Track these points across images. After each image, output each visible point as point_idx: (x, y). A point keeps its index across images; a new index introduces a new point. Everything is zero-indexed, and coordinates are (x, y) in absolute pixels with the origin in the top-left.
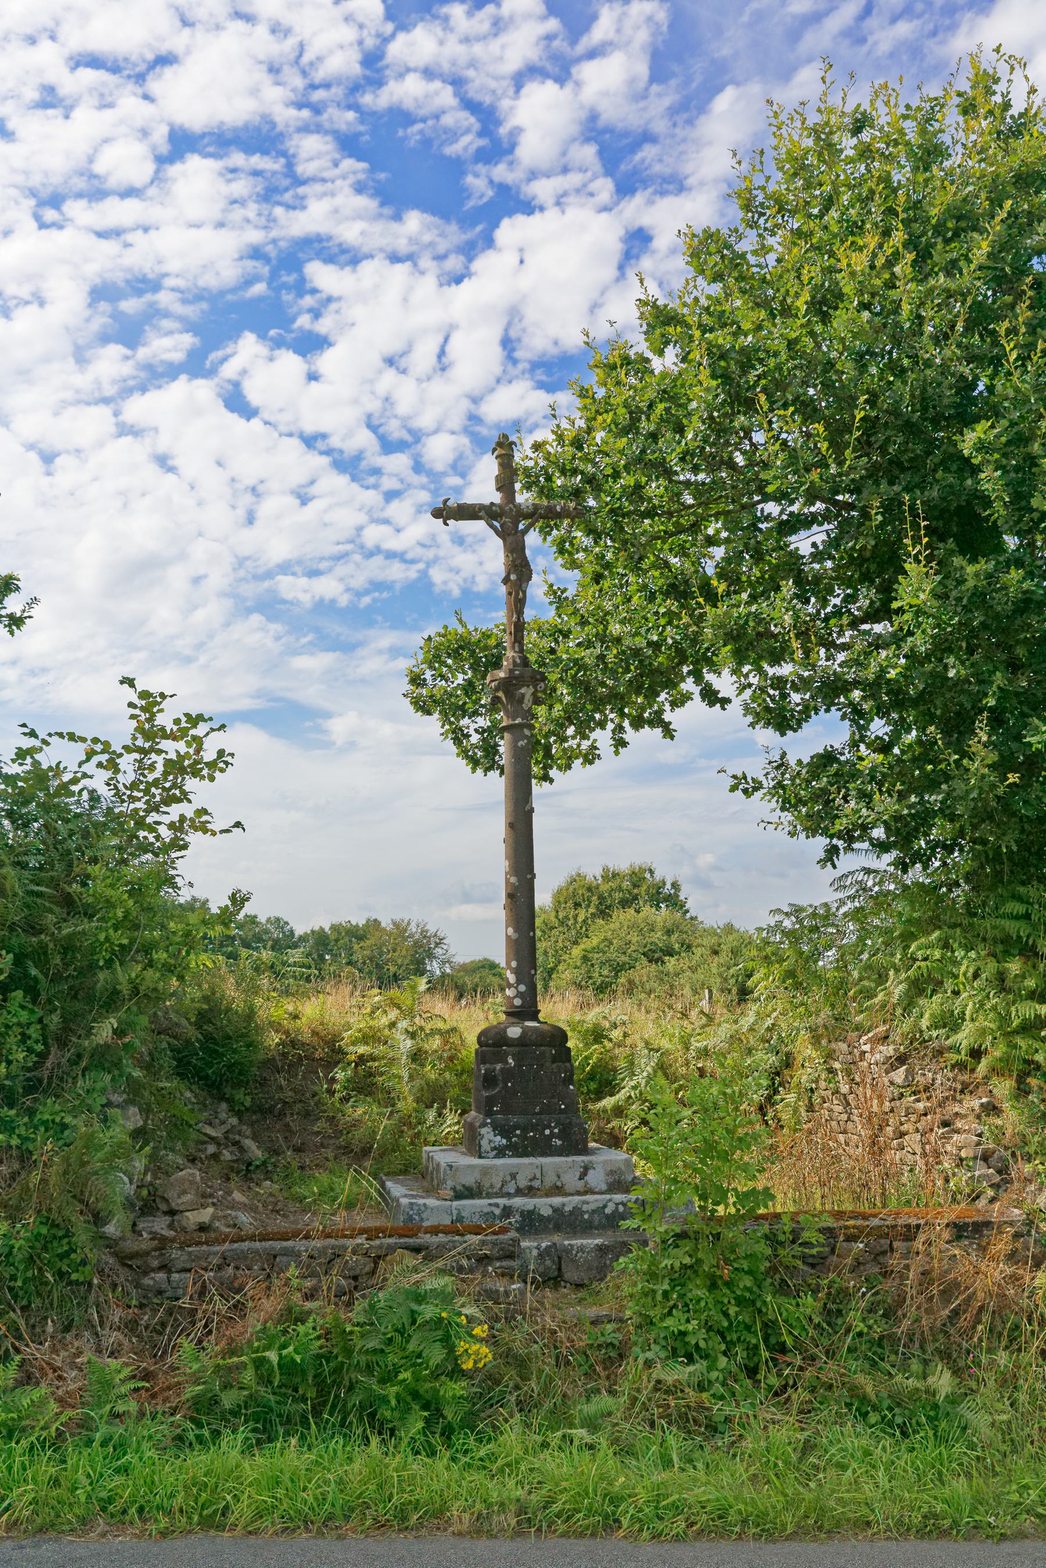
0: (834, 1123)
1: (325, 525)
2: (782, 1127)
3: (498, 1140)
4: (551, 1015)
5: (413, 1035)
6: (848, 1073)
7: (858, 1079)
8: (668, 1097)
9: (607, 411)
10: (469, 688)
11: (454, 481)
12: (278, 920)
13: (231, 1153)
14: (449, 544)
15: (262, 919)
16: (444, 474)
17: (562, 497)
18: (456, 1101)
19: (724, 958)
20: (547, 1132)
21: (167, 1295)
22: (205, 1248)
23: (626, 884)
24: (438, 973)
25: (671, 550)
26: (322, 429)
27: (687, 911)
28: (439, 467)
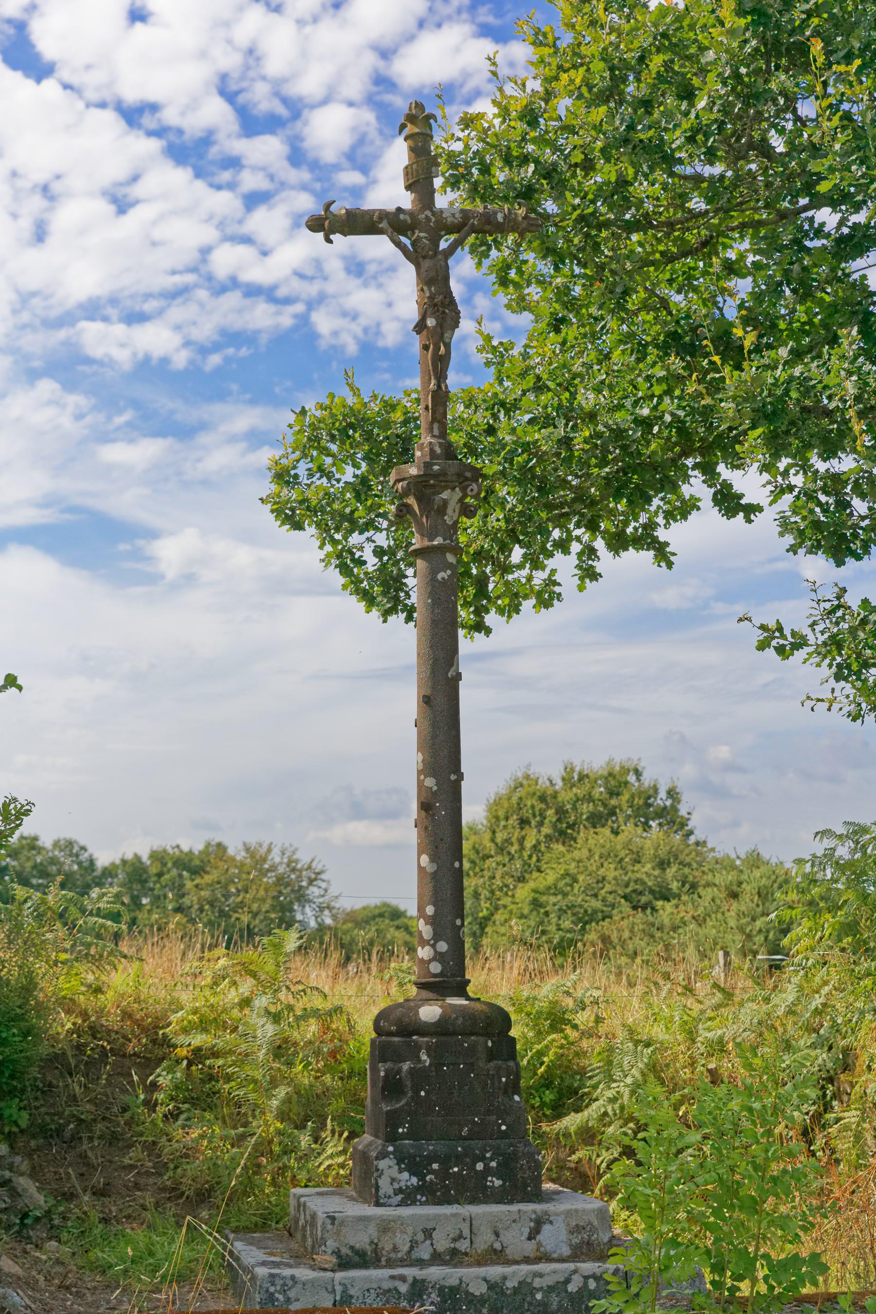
1: (154, 244)
2: (837, 1162)
3: (408, 1179)
4: (486, 988)
5: (276, 1018)
8: (665, 1113)
9: (575, 67)
10: (361, 490)
11: (351, 178)
12: (70, 844)
14: (342, 275)
15: (46, 841)
16: (336, 167)
17: (505, 198)
18: (341, 1119)
19: (747, 902)
20: (480, 1166)
23: (600, 791)
24: (313, 924)
25: (670, 281)
26: (152, 95)
27: (691, 833)
28: (329, 156)
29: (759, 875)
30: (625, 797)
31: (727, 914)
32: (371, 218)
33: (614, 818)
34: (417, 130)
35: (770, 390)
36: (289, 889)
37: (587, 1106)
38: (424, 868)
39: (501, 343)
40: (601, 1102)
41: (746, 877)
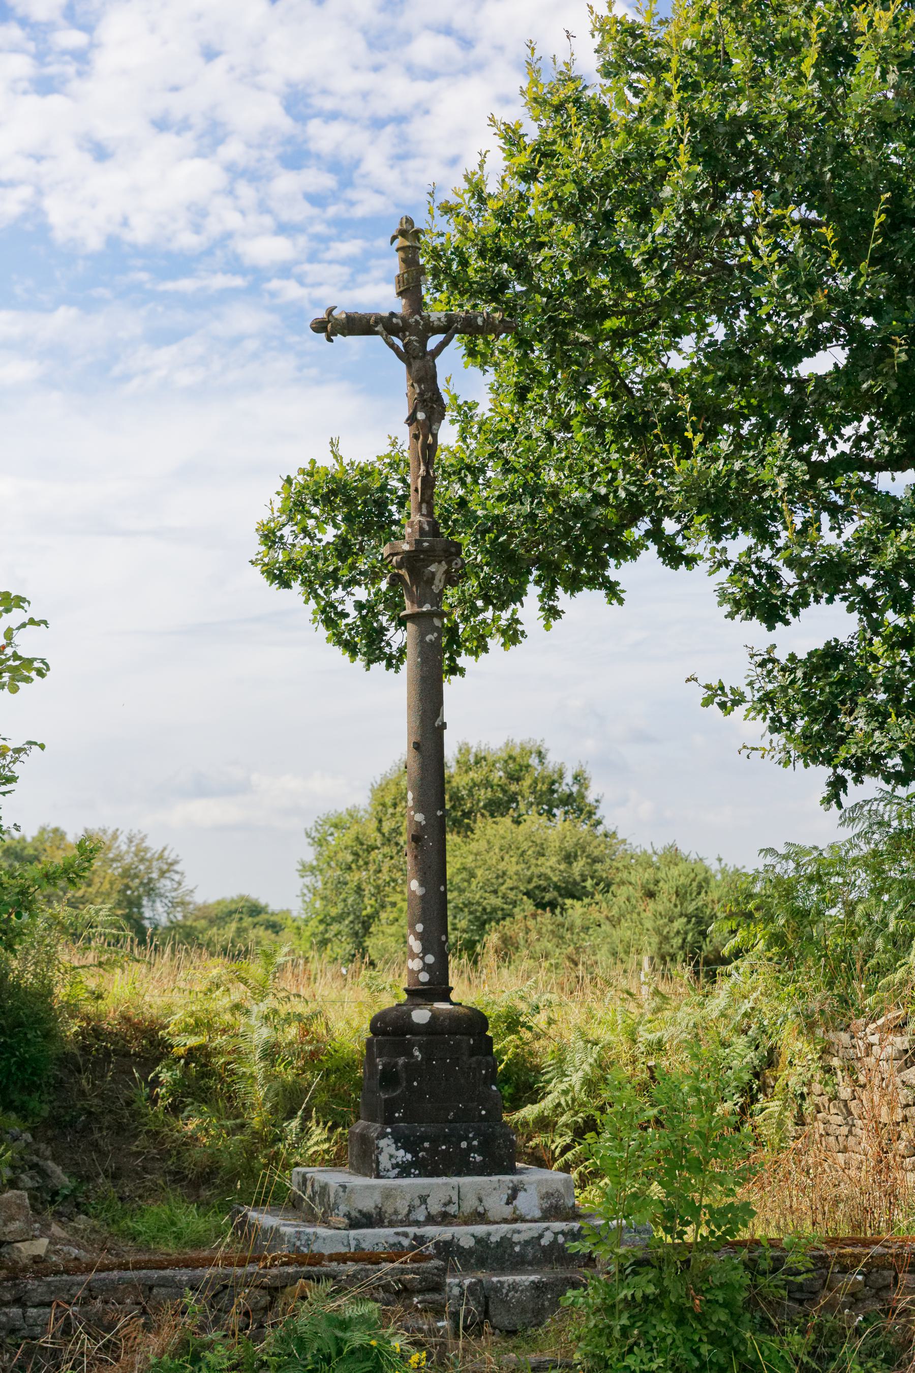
0: (832, 1139)
3: (403, 1156)
6: (851, 1070)
7: (862, 1079)
13: (32, 1178)
19: (663, 903)
20: (464, 1145)
21: (23, 1333)
22: (65, 1277)
23: (498, 775)
27: (599, 823)
29: (677, 873)
30: (527, 782)
31: (643, 915)
32: (368, 321)
33: (514, 805)
34: (407, 243)
35: (713, 482)
36: (137, 881)
37: (543, 1098)
38: (414, 892)
39: (466, 402)
40: (556, 1094)
41: (664, 875)
